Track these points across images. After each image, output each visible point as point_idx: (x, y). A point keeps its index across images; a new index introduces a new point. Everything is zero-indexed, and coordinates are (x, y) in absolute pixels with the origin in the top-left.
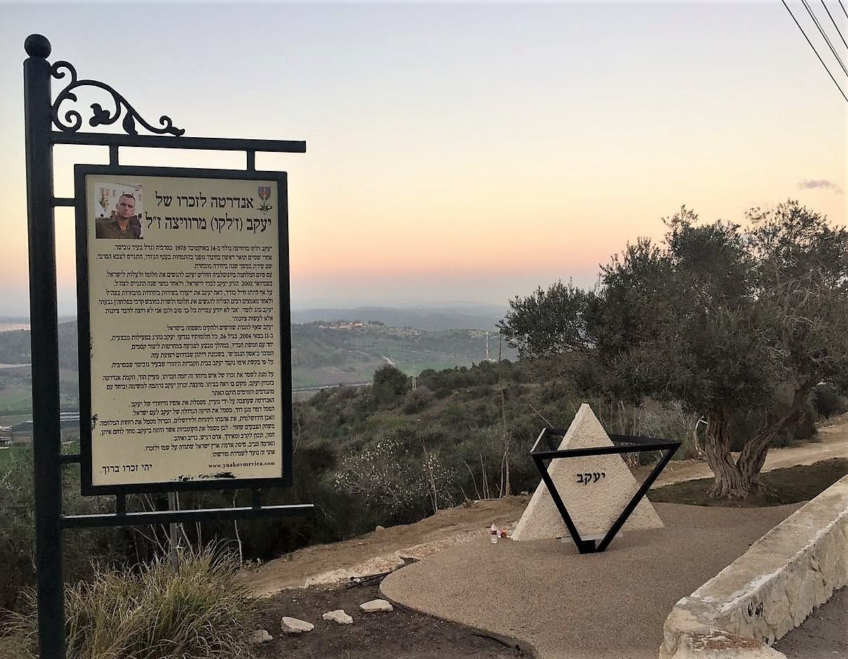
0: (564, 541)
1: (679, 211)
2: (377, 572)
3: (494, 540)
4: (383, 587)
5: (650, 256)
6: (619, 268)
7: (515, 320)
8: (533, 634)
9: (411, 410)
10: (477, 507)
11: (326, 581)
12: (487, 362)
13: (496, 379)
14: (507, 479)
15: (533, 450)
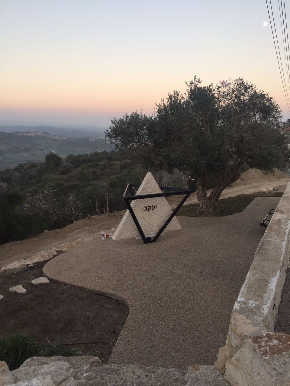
0: (137, 238)
1: (193, 78)
2: (42, 260)
3: (103, 239)
4: (45, 270)
5: (178, 101)
6: (164, 106)
7: (114, 130)
8: (125, 291)
9: (62, 173)
10: (94, 219)
11: (12, 267)
12: (97, 152)
13: (102, 159)
14: (108, 205)
15: (124, 195)
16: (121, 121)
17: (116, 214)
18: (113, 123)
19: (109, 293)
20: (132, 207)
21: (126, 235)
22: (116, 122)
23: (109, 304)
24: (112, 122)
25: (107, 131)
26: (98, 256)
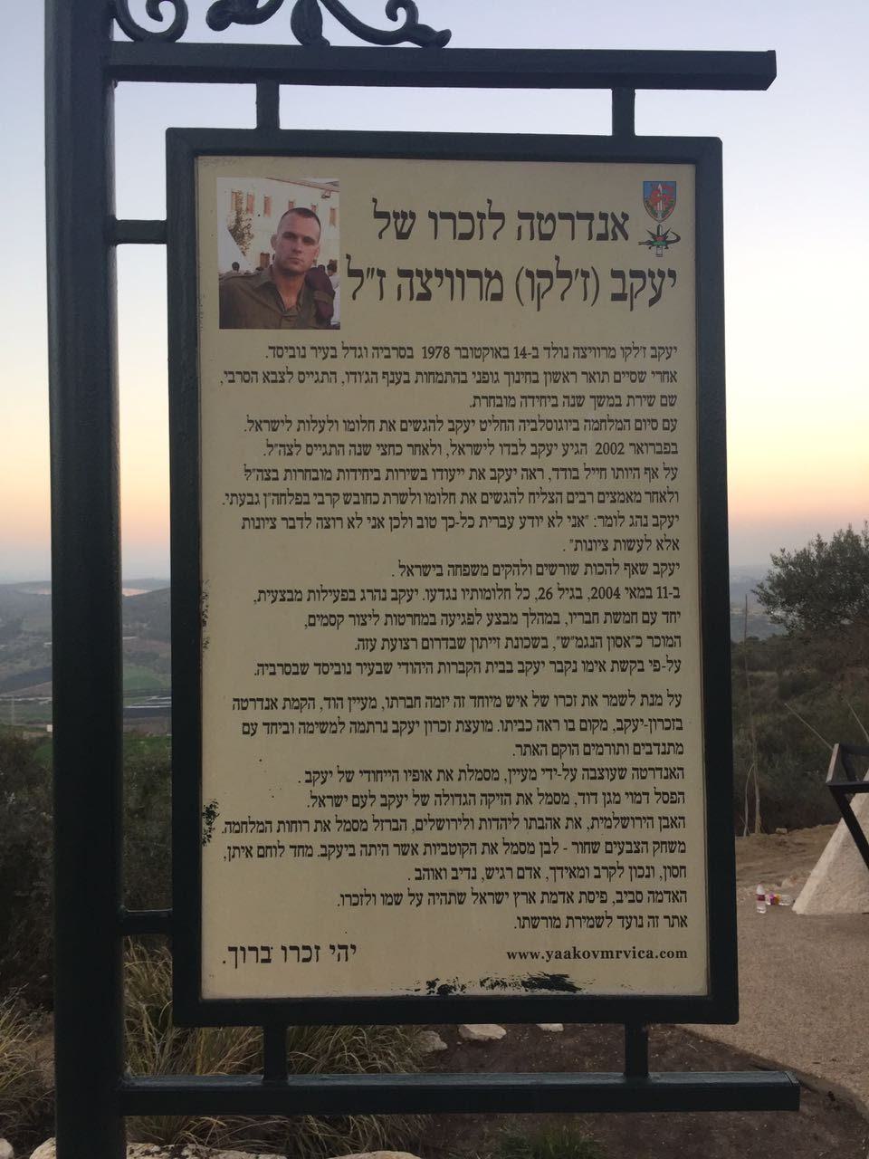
7: (778, 583)
8: (853, 1073)
15: (829, 778)
16: (803, 558)
17: (786, 838)
18: (776, 563)
19: (803, 1071)
20: (856, 814)
21: (837, 901)
22: (786, 561)
23: (808, 1104)
24: (776, 561)
25: (761, 587)
26: (754, 959)
